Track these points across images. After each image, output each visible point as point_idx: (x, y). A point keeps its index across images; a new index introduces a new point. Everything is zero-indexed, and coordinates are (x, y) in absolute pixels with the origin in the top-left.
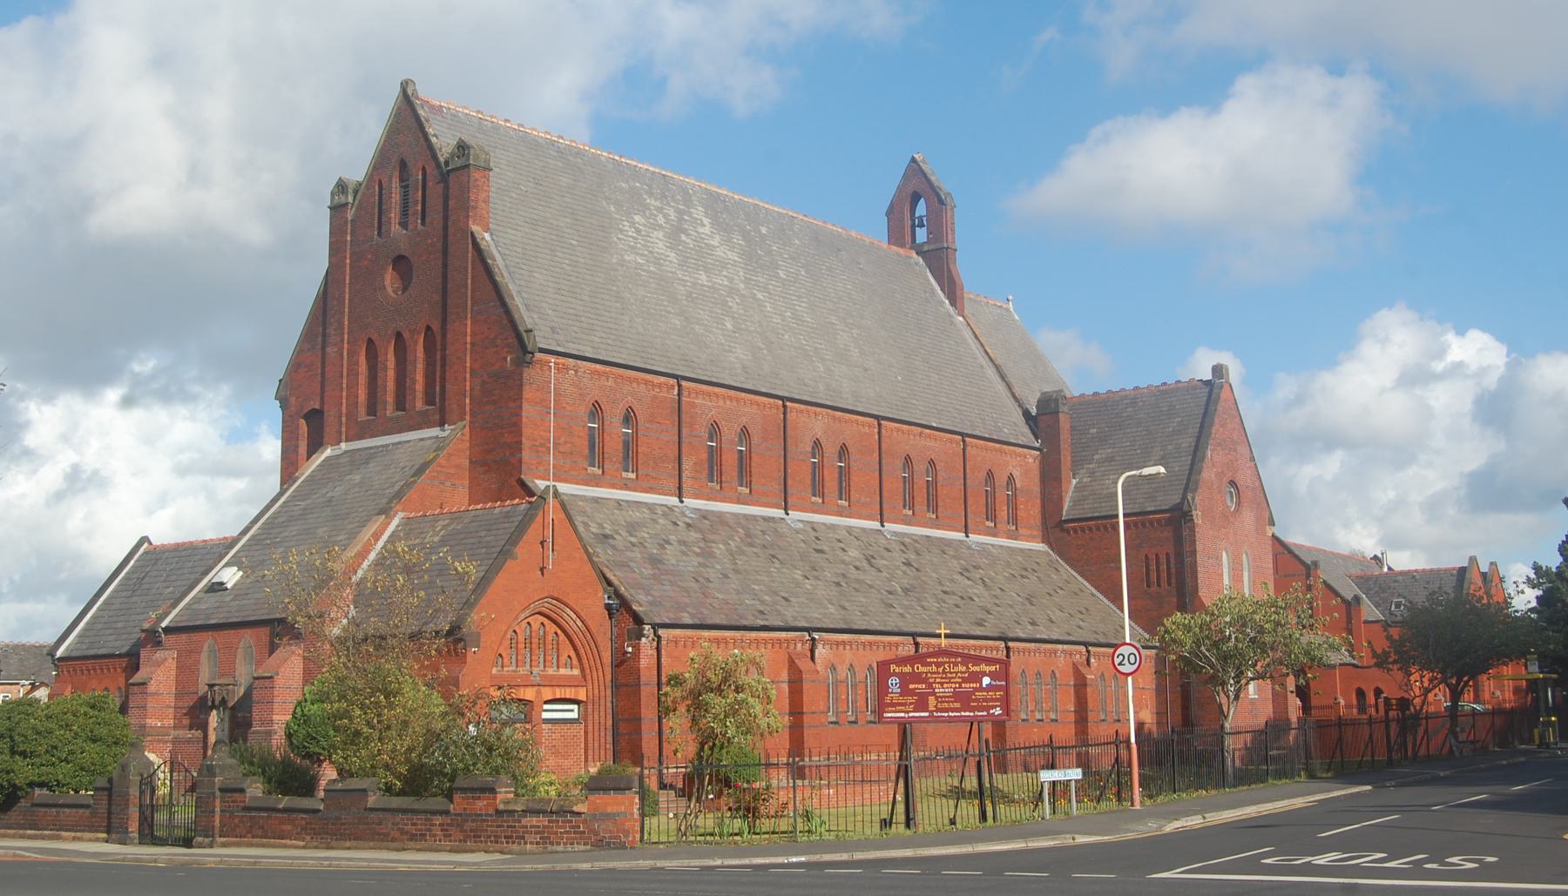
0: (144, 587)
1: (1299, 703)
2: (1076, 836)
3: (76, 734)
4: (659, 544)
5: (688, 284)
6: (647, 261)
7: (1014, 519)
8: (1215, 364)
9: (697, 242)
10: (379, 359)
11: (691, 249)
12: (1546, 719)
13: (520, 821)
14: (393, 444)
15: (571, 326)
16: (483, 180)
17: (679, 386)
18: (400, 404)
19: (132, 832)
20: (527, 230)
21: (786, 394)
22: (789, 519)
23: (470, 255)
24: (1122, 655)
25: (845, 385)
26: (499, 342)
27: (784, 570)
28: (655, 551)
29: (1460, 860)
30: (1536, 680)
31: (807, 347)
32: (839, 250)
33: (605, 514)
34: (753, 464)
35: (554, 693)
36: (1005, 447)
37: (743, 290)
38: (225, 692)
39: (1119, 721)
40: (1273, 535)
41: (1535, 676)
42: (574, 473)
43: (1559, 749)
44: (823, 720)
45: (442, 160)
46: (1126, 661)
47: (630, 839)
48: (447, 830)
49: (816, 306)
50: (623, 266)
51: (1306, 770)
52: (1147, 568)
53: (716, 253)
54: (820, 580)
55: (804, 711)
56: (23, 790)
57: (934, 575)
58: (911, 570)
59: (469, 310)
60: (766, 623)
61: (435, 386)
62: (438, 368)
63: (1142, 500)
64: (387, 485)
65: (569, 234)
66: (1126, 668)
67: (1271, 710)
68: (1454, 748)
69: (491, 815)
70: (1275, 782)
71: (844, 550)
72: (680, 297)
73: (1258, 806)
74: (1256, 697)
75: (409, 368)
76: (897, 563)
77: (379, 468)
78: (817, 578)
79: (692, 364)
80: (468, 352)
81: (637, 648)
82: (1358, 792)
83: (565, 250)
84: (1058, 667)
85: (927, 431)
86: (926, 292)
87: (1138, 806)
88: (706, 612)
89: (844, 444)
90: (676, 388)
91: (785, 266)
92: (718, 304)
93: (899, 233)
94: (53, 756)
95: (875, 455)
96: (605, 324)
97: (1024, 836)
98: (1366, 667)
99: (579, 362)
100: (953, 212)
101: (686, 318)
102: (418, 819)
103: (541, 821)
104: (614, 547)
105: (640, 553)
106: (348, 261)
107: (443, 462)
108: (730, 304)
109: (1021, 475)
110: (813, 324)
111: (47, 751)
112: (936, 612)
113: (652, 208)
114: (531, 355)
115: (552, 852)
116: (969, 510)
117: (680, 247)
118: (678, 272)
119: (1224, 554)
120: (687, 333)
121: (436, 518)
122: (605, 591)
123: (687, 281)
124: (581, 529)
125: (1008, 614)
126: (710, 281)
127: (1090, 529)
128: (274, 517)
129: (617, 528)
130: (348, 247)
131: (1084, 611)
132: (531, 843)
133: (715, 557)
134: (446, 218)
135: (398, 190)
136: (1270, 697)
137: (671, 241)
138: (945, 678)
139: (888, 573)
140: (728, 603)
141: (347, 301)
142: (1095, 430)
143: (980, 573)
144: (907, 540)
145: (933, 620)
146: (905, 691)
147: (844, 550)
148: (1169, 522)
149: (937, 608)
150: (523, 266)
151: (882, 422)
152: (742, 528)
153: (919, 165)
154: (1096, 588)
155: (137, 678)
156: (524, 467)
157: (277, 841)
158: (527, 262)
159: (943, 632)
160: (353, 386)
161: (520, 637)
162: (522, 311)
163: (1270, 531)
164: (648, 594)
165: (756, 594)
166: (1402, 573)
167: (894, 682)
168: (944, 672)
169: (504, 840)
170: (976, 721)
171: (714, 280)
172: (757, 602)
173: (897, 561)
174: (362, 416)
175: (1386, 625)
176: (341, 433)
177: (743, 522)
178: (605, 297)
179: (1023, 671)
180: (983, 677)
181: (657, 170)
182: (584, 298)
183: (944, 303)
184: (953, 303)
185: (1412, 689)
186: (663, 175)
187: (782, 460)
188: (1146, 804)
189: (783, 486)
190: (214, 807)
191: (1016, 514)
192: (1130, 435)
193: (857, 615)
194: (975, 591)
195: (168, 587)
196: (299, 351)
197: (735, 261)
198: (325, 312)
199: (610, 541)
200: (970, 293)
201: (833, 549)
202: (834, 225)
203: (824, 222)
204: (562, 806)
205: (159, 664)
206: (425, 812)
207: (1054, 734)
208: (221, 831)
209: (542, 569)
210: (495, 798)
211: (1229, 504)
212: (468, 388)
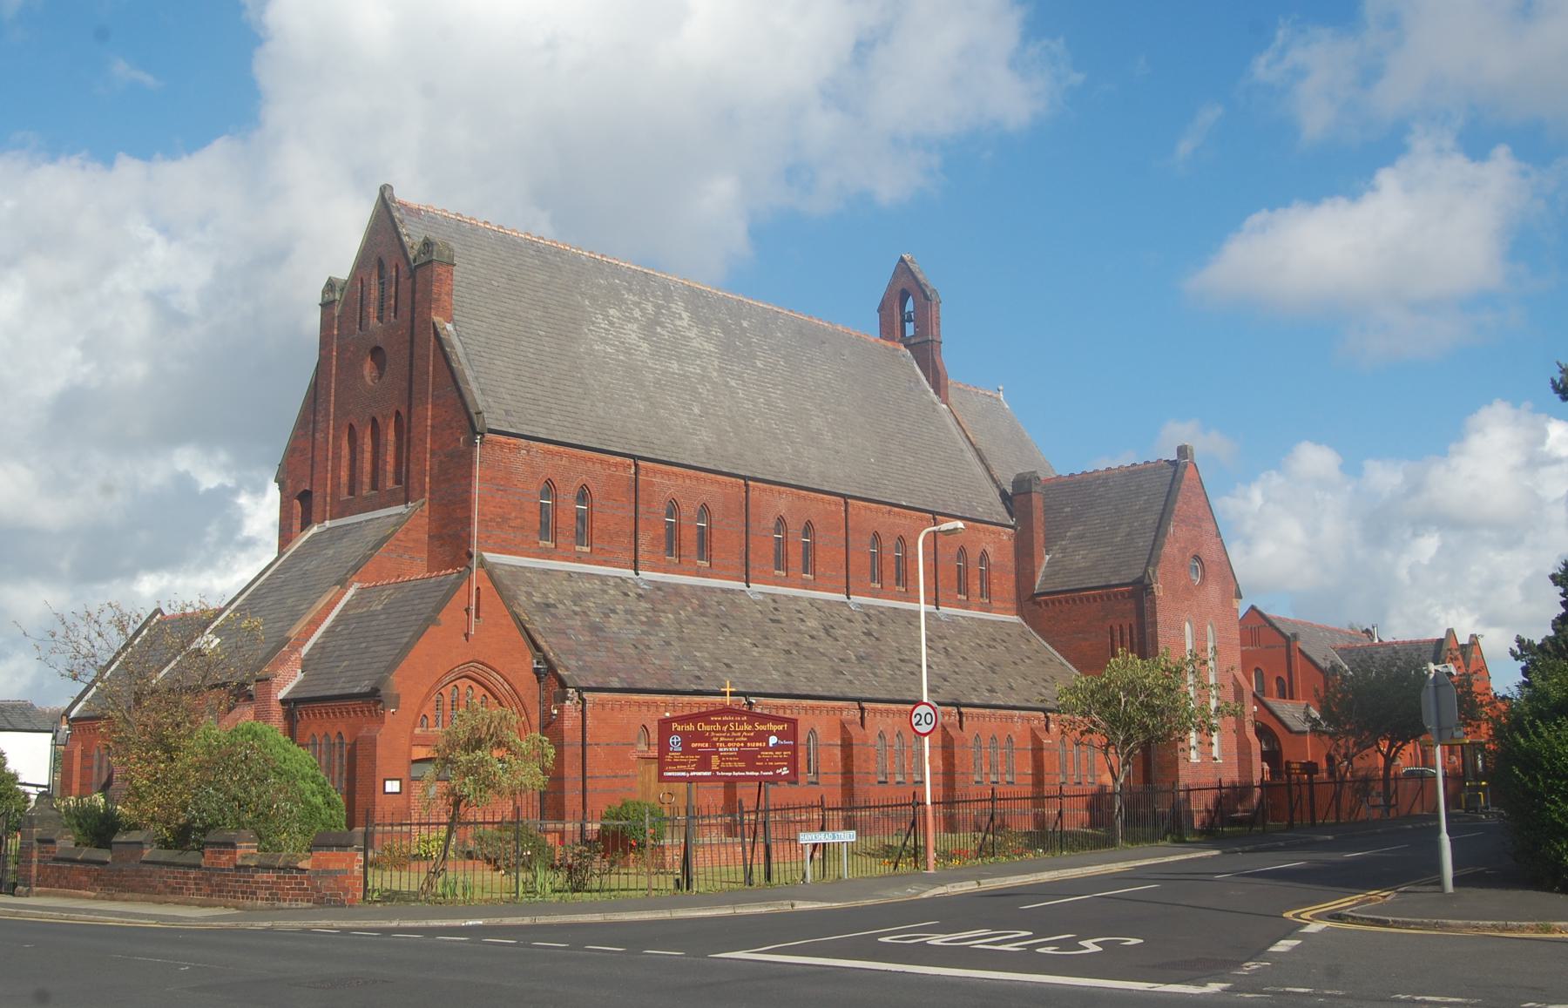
4: (604, 613)
5: (658, 372)
6: (617, 351)
7: (986, 592)
8: (1180, 445)
10: (358, 443)
11: (665, 340)
12: (1473, 783)
13: (253, 877)
14: (366, 521)
15: (527, 409)
16: (446, 274)
17: (636, 465)
18: (374, 486)
20: (494, 322)
21: (748, 474)
23: (432, 344)
24: (919, 714)
28: (597, 620)
32: (824, 343)
33: (552, 584)
37: (716, 378)
39: (1080, 783)
45: (411, 257)
46: (922, 721)
47: (350, 897)
50: (590, 355)
53: (691, 344)
54: (770, 648)
57: (894, 644)
59: (430, 396)
60: (700, 688)
62: (405, 450)
63: (1107, 574)
65: (538, 325)
66: (924, 729)
67: (1237, 774)
69: (231, 870)
71: (802, 620)
72: (648, 384)
73: (1060, 871)
74: (1199, 761)
75: (381, 450)
76: (856, 633)
77: (350, 543)
78: (767, 646)
79: (652, 445)
80: (429, 435)
81: (561, 709)
84: (1015, 732)
85: (896, 509)
86: (910, 381)
87: (932, 871)
88: (637, 676)
89: (809, 521)
90: (633, 467)
91: (764, 357)
92: (686, 390)
95: (841, 531)
99: (531, 442)
100: (938, 307)
101: (651, 403)
103: (270, 877)
104: (554, 616)
106: (335, 354)
108: (701, 390)
109: (994, 551)
110: (786, 409)
112: (888, 679)
113: (629, 302)
115: (278, 909)
116: (939, 584)
117: (655, 339)
119: (1187, 624)
120: (650, 417)
122: (534, 656)
123: (657, 369)
127: (1060, 602)
128: (257, 589)
129: (561, 598)
130: (335, 341)
131: (1049, 678)
132: (262, 899)
133: (661, 626)
134: (413, 310)
137: (646, 333)
138: (729, 737)
139: (845, 642)
140: (663, 669)
142: (1069, 509)
143: (944, 643)
144: (872, 611)
146: (687, 750)
147: (802, 620)
148: (1132, 595)
149: (891, 675)
150: (483, 354)
151: (849, 500)
152: (698, 600)
153: (907, 265)
154: (1066, 658)
157: (73, 891)
159: (728, 690)
160: (337, 467)
165: (697, 661)
167: (675, 740)
168: (728, 731)
169: (240, 895)
172: (696, 668)
173: (857, 631)
176: (325, 511)
177: (699, 593)
178: (568, 383)
181: (639, 269)
182: (545, 384)
183: (929, 391)
184: (937, 392)
186: (646, 273)
187: (744, 536)
190: (32, 857)
191: (990, 589)
192: (1101, 513)
194: (935, 659)
196: (295, 438)
197: (710, 351)
198: (315, 400)
199: (552, 610)
201: (790, 619)
202: (820, 320)
204: (289, 862)
206: (183, 865)
208: (38, 880)
209: (467, 635)
210: (235, 853)
211: (1194, 578)
212: (428, 468)
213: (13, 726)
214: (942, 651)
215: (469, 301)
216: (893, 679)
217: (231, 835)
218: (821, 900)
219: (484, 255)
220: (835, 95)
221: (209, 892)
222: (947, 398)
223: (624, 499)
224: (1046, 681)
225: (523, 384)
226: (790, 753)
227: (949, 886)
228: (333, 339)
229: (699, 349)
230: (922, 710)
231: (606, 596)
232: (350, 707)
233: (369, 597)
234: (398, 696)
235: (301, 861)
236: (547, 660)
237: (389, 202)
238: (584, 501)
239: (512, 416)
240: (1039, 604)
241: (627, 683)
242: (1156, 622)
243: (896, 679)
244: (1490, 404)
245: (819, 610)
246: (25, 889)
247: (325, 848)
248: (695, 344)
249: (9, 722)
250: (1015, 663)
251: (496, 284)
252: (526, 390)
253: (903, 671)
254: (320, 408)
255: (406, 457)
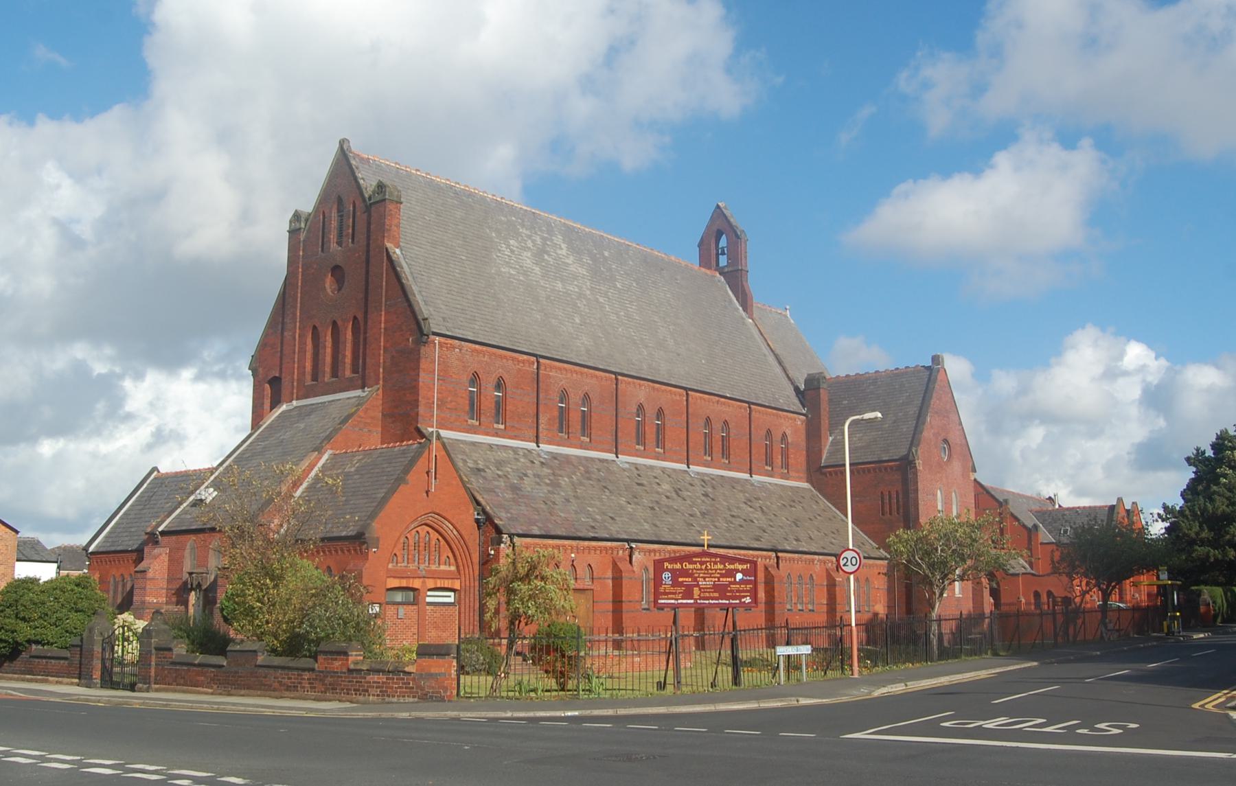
0: (152, 502)
1: (992, 601)
2: (800, 699)
3: (62, 605)
4: (519, 477)
5: (548, 290)
6: (518, 273)
8: (934, 354)
9: (556, 260)
10: (321, 340)
11: (551, 265)
12: (1172, 614)
13: (365, 678)
14: (329, 402)
15: (458, 317)
17: (538, 362)
18: (335, 373)
19: (96, 679)
20: (429, 248)
21: (618, 371)
22: (619, 461)
23: (385, 264)
24: (847, 559)
25: (662, 365)
26: (404, 328)
27: (613, 497)
28: (516, 482)
29: (1107, 726)
30: (1165, 585)
31: (635, 338)
32: (663, 270)
34: (593, 421)
35: (436, 583)
36: (780, 413)
38: (200, 578)
40: (975, 480)
41: (1165, 582)
42: (458, 423)
43: (1181, 636)
44: (639, 607)
45: (367, 196)
46: (849, 563)
47: (448, 694)
48: (313, 684)
49: (643, 308)
50: (499, 275)
51: (992, 649)
52: (882, 502)
54: (639, 505)
55: (624, 599)
56: (24, 645)
57: (725, 503)
58: (708, 500)
59: (383, 305)
60: (596, 535)
61: (359, 359)
62: (361, 347)
63: (879, 452)
64: (321, 431)
65: (460, 252)
66: (850, 569)
68: (1104, 635)
69: (345, 673)
70: (967, 658)
71: (658, 484)
72: (541, 299)
74: (961, 596)
75: (341, 346)
76: (697, 495)
78: (637, 504)
80: (382, 335)
81: (497, 551)
82: (1029, 667)
83: (457, 263)
84: (815, 572)
87: (856, 676)
90: (536, 364)
91: (622, 280)
92: (569, 304)
93: (707, 260)
94: (45, 621)
96: (484, 317)
97: (758, 699)
98: (1042, 576)
99: (463, 343)
102: (292, 674)
104: (484, 478)
105: (504, 482)
106: (300, 270)
107: (362, 414)
108: (579, 305)
110: (640, 321)
111: (40, 617)
112: (725, 530)
113: (523, 235)
114: (426, 337)
115: (388, 703)
116: (753, 458)
117: (543, 264)
118: (541, 281)
119: (939, 491)
121: (354, 454)
122: (475, 509)
123: (547, 288)
124: (460, 464)
125: (779, 533)
126: (565, 288)
128: (245, 450)
129: (487, 464)
130: (301, 260)
131: (836, 532)
132: (374, 695)
133: (560, 487)
134: (368, 238)
135: (336, 219)
136: (971, 596)
138: (707, 574)
139: (691, 502)
141: (299, 299)
142: (846, 402)
144: (706, 478)
145: (723, 536)
146: (675, 583)
147: (658, 484)
150: (423, 273)
151: (689, 392)
152: (583, 466)
155: (141, 567)
156: (420, 418)
157: (190, 688)
158: (427, 271)
161: (410, 541)
162: (421, 306)
163: (973, 476)
164: (507, 512)
165: (590, 515)
166: (1068, 509)
167: (667, 576)
168: (706, 569)
169: (353, 693)
170: (731, 607)
171: (568, 288)
172: (591, 520)
174: (309, 382)
175: (1058, 544)
176: (293, 394)
177: (584, 462)
178: (485, 297)
179: (789, 574)
180: (736, 573)
182: (469, 297)
183: (738, 309)
184: (745, 310)
185: (1074, 591)
186: (534, 213)
188: (864, 673)
189: (614, 437)
190: (151, 661)
193: (665, 531)
195: (167, 503)
196: (266, 335)
198: (284, 305)
199: (482, 473)
200: (758, 303)
202: (659, 252)
203: (652, 250)
204: (397, 667)
205: (156, 557)
206: (297, 669)
207: (789, 618)
208: (156, 679)
209: (427, 492)
210: (347, 660)
211: (943, 456)
212: (381, 361)
213: (27, 557)
214: (759, 509)
215: (410, 231)
216: (728, 530)
217: (342, 646)
218: (816, 698)
219: (418, 195)
220: (588, 84)
221: (323, 689)
222: (752, 315)
223: (528, 388)
224: (833, 533)
225: (454, 297)
226: (751, 586)
227: (889, 686)
228: (299, 259)
229: (575, 272)
230: (848, 554)
231: (518, 463)
232: (338, 548)
233: (341, 462)
234: (378, 539)
235: (408, 666)
236: (484, 512)
237: (347, 152)
238: (500, 389)
239: (448, 322)
240: (825, 474)
241: (544, 531)
242: (917, 490)
243: (730, 530)
244: (1083, 328)
245: (669, 476)
246: (145, 686)
247: (427, 657)
248: (572, 268)
249: (23, 555)
250: (810, 519)
251: (428, 219)
252: (457, 302)
253: (734, 524)
254: (288, 312)
255: (363, 352)
